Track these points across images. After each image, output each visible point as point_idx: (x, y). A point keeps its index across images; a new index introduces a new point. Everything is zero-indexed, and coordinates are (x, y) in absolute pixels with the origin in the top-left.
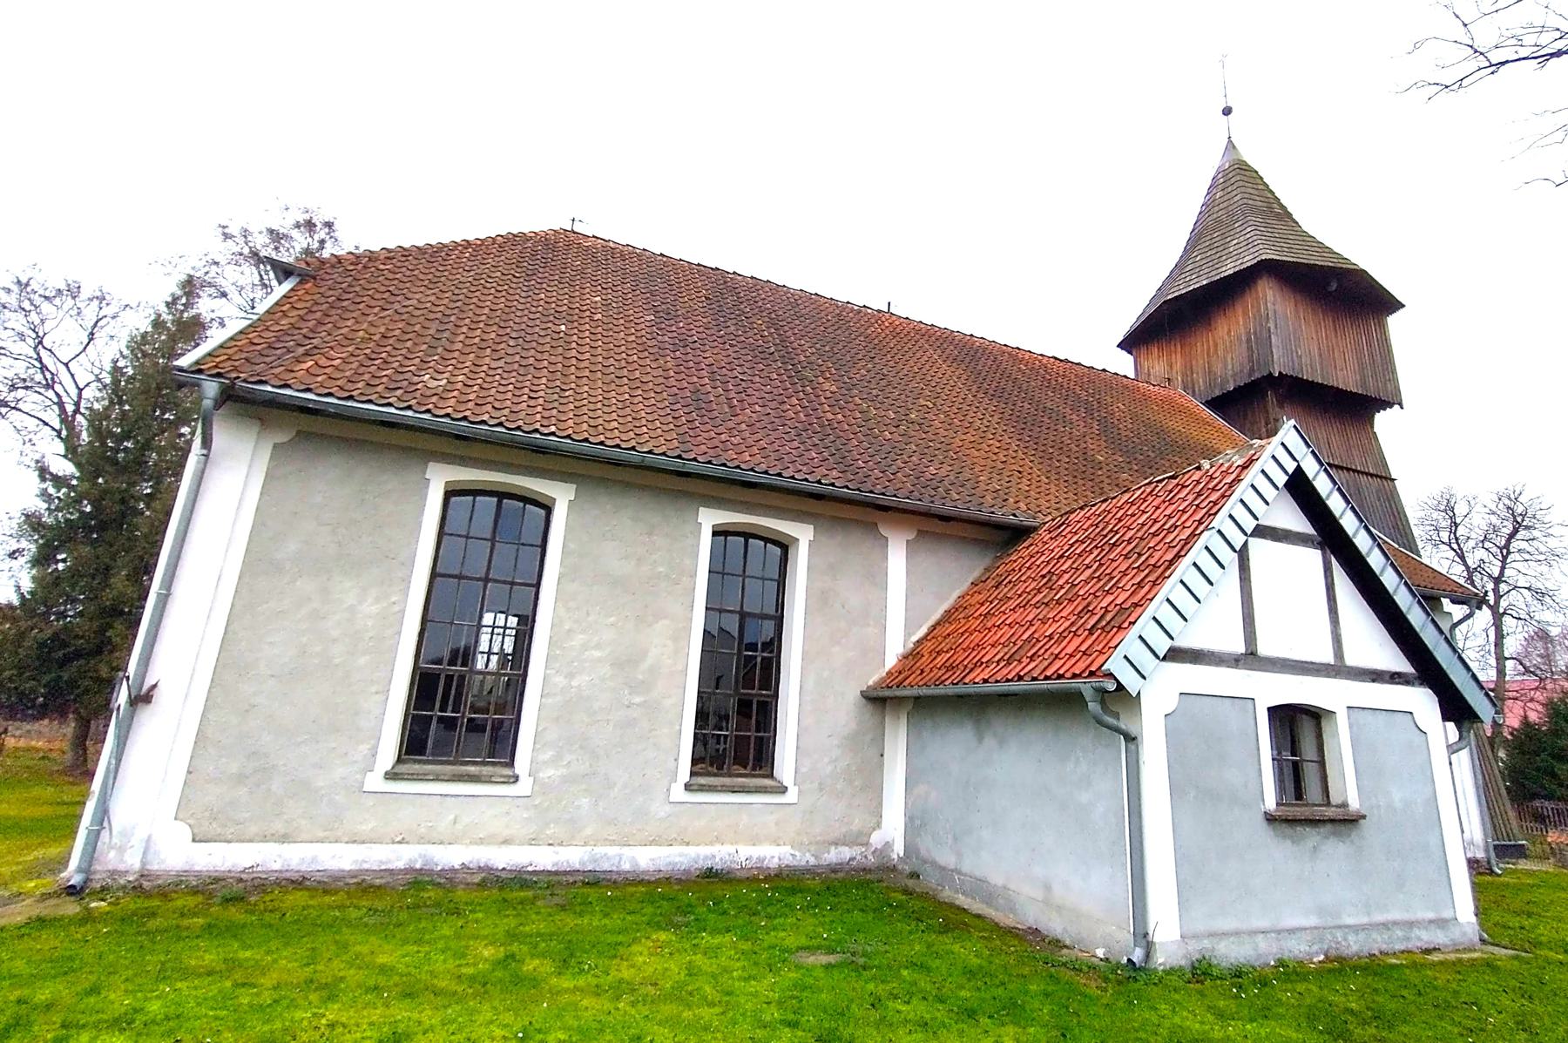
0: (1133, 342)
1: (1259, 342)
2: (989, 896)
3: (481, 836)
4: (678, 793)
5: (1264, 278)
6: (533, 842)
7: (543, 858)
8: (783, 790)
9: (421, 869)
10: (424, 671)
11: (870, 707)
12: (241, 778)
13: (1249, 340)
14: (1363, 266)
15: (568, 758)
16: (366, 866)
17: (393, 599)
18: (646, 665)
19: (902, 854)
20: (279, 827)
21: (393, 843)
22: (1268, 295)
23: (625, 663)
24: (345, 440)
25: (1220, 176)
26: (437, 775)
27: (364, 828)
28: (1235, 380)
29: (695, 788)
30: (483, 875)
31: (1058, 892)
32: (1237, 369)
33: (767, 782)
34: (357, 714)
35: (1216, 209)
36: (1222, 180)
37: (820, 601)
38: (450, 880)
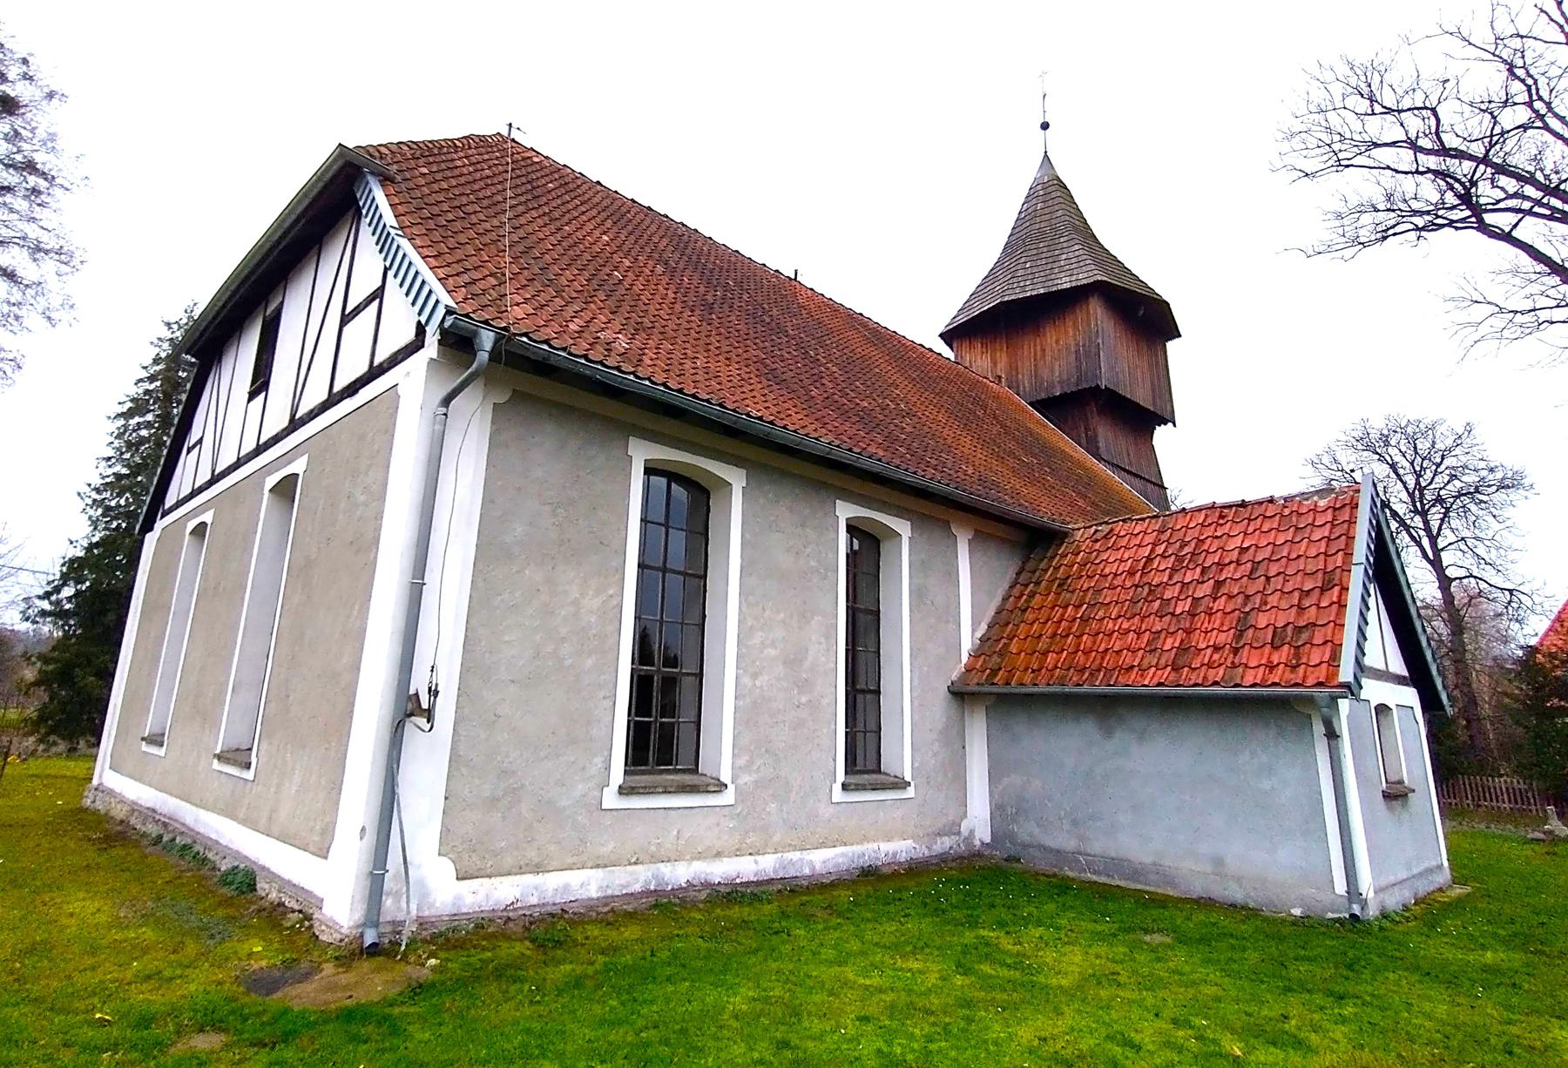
0: (948, 337)
1: (1088, 354)
2: (1136, 872)
3: (700, 850)
4: (838, 794)
5: (1096, 297)
6: (738, 853)
7: (745, 868)
8: (901, 784)
9: (655, 891)
10: (666, 675)
11: (950, 696)
12: (493, 802)
13: (1077, 352)
14: (1165, 298)
15: (759, 762)
16: (609, 892)
17: (611, 592)
18: (807, 664)
19: (988, 839)
20: (532, 855)
21: (630, 864)
22: (1097, 313)
23: (793, 661)
24: (557, 405)
25: (1039, 187)
26: (665, 787)
27: (605, 849)
28: (1062, 387)
29: (853, 787)
30: (708, 891)
31: (1233, 866)
32: (1065, 377)
33: (688, 779)
34: (589, 723)
35: (1038, 220)
36: (1041, 193)
37: (917, 593)
38: (683, 900)
